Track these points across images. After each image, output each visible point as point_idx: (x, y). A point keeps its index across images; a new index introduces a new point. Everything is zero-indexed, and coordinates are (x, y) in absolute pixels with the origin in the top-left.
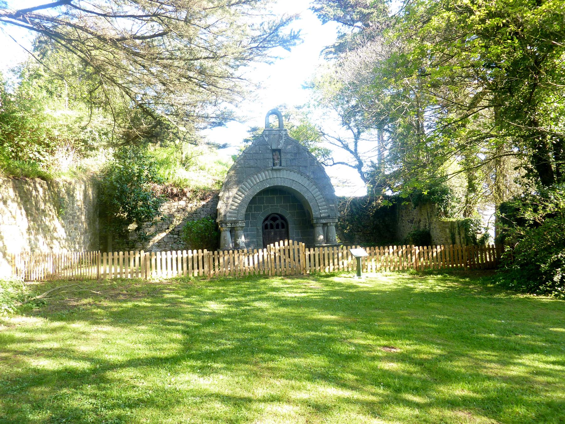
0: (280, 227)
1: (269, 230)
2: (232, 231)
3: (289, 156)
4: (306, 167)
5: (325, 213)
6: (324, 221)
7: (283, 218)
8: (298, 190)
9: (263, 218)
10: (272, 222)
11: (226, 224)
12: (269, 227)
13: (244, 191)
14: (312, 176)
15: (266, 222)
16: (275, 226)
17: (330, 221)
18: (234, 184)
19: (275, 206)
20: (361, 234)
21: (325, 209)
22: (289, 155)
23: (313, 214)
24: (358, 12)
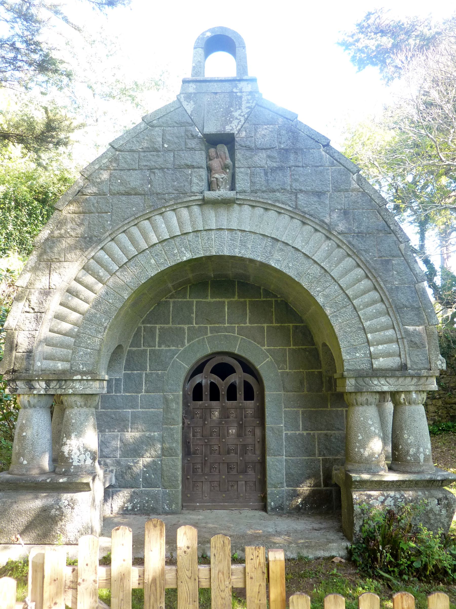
0: (240, 394)
1: (206, 402)
2: (56, 407)
3: (261, 159)
4: (319, 194)
5: (388, 355)
6: (385, 385)
7: (248, 368)
8: (292, 273)
9: (186, 367)
10: (215, 379)
11: (29, 382)
12: (206, 392)
13: (102, 272)
14: (341, 227)
15: (198, 379)
16: (223, 392)
17: (409, 384)
18: (71, 248)
19: (226, 329)
20: (440, 403)
21: (389, 341)
22: (263, 155)
23: (345, 356)
24: (417, 36)
